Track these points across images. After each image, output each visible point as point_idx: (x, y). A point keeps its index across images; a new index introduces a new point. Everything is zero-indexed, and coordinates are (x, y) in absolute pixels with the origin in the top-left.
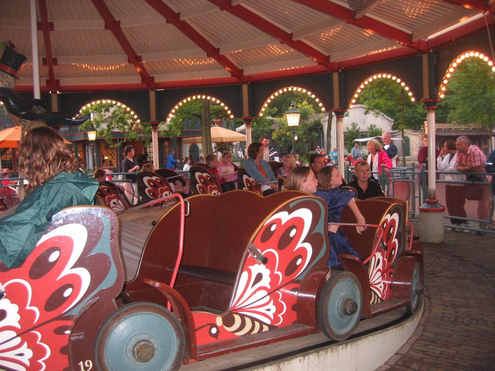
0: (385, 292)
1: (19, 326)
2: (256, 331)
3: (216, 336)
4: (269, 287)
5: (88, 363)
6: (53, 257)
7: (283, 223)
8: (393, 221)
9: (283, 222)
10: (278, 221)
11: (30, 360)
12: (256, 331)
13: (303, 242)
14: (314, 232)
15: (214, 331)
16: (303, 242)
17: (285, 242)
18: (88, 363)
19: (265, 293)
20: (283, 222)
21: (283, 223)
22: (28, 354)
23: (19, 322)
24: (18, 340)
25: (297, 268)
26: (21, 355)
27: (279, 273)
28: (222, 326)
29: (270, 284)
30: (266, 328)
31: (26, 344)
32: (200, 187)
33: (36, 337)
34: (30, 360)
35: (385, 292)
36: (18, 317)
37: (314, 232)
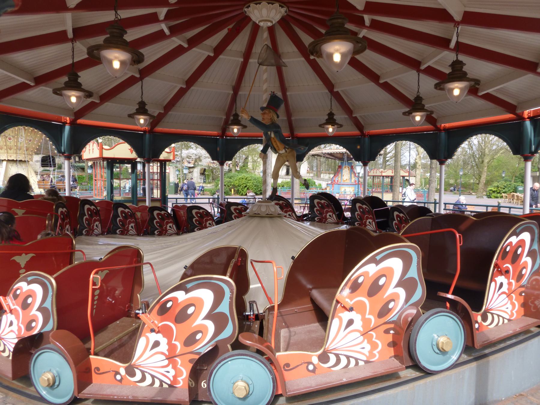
0: (514, 301)
1: (167, 353)
2: (501, 323)
3: (313, 371)
4: (362, 330)
5: (204, 385)
6: (190, 310)
7: (370, 275)
8: (522, 243)
9: (371, 274)
10: (365, 274)
11: (173, 376)
12: (501, 323)
13: (395, 287)
14: (406, 277)
15: (311, 367)
16: (395, 287)
17: (375, 289)
18: (204, 385)
19: (358, 334)
20: (371, 274)
21: (370, 275)
22: (172, 372)
23: (168, 350)
24: (166, 362)
25: (389, 310)
26: (168, 372)
27: (371, 317)
28: (318, 363)
29: (362, 326)
30: (506, 321)
31: (171, 366)
32: (120, 221)
33: (372, 336)
34: (173, 376)
35: (514, 301)
36: (167, 347)
37: (406, 277)
